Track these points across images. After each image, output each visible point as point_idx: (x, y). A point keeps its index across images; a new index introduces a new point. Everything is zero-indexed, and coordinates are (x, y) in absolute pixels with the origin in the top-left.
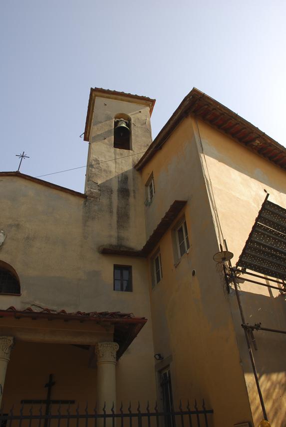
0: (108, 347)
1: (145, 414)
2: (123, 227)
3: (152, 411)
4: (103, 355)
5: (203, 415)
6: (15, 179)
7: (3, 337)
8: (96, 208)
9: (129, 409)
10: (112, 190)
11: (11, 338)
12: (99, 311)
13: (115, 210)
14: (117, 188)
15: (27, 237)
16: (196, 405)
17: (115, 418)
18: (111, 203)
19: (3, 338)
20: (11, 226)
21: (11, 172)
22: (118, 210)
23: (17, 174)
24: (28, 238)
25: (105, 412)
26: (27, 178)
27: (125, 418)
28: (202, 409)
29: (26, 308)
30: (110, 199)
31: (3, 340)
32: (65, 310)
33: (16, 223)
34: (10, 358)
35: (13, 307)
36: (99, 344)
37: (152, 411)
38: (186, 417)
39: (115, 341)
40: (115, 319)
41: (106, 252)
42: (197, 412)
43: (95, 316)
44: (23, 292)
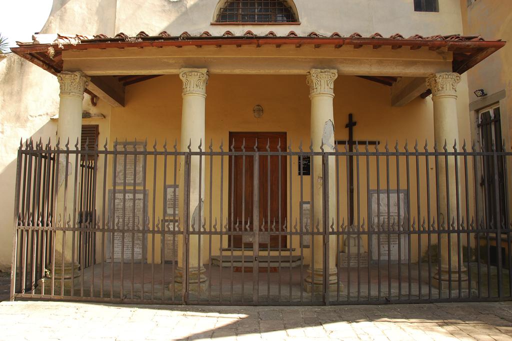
0: (448, 78)
1: (373, 153)
3: (469, 149)
7: (326, 70)
9: (425, 148)
11: (335, 71)
12: (443, 35)
17: (458, 157)
19: (325, 72)
25: (190, 150)
27: (410, 157)
29: (202, 32)
31: (327, 73)
32: (231, 31)
34: (206, 93)
35: (187, 33)
36: (438, 75)
38: (451, 159)
39: (454, 71)
40: (464, 43)
42: (407, 154)
43: (439, 39)
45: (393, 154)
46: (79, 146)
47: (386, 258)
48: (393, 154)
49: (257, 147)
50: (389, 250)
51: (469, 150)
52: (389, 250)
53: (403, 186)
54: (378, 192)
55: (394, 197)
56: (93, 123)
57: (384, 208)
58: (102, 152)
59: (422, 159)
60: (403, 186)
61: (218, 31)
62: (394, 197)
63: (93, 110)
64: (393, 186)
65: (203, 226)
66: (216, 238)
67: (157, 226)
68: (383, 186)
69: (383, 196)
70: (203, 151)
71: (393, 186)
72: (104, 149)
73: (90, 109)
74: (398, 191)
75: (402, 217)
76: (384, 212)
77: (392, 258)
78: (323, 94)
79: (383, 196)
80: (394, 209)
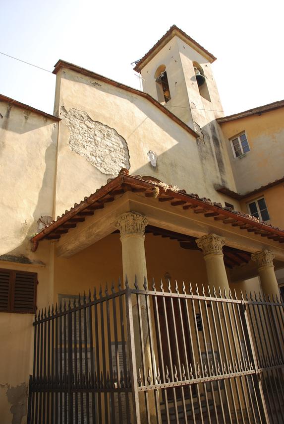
26: (156, 103)
56: (31, 270)
63: (31, 256)
73: (28, 254)
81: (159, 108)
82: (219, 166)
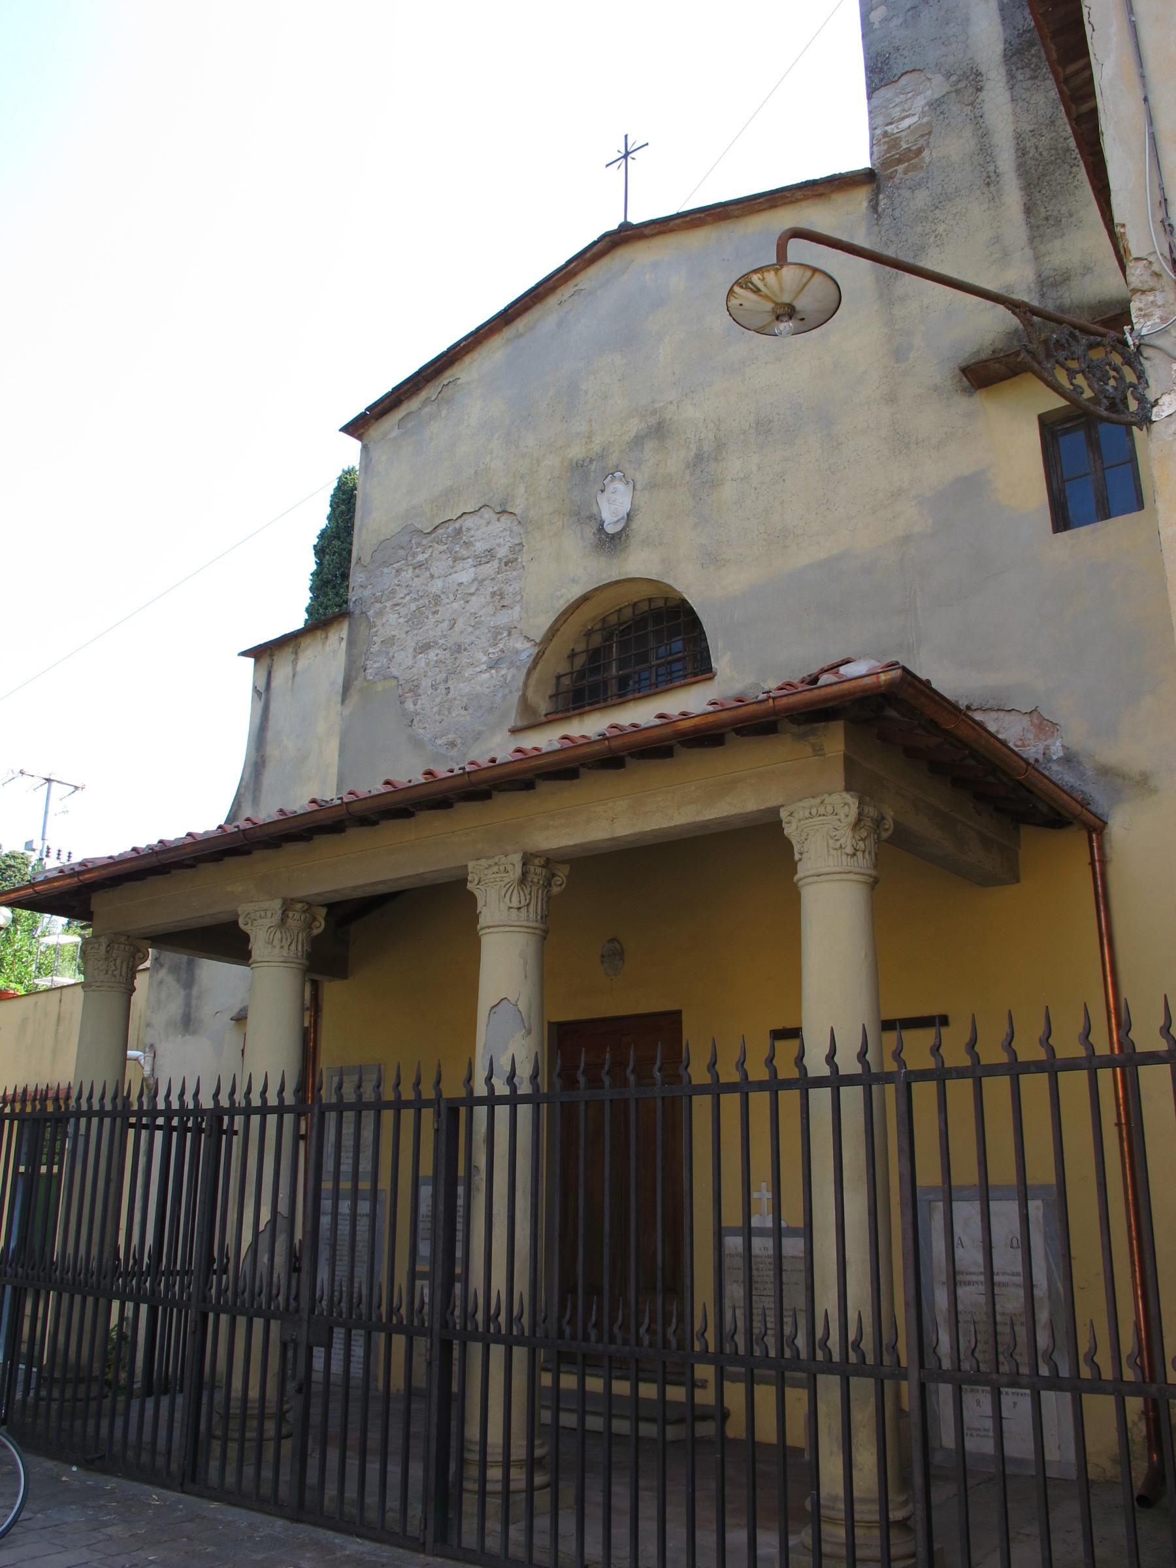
1: (1035, 1063)
2: (1058, 221)
3: (848, 1064)
4: (801, 854)
5: (1005, 1081)
6: (640, 255)
8: (921, 198)
10: (979, 74)
13: (1006, 161)
14: (999, 47)
15: (696, 456)
16: (973, 1042)
18: (983, 136)
20: (638, 441)
21: (595, 243)
22: (1021, 152)
23: (625, 236)
24: (699, 458)
26: (647, 231)
28: (791, 1073)
30: (978, 120)
33: (652, 421)
37: (848, 1064)
41: (983, 375)
42: (1015, 1069)
44: (721, 662)
45: (761, 1086)
46: (543, 1080)
47: (988, 1446)
48: (761, 1086)
49: (660, 1070)
50: (998, 1418)
51: (524, 1088)
52: (998, 1418)
53: (1041, 1172)
54: (949, 1195)
55: (1005, 1213)
57: (970, 1256)
58: (702, 1090)
59: (1034, 1086)
60: (1041, 1172)
61: (546, 740)
62: (1005, 1213)
64: (1002, 1171)
65: (1049, 1359)
66: (1099, 1407)
67: (1049, 1359)
68: (965, 1172)
69: (967, 1212)
70: (1102, 1049)
71: (1002, 1171)
72: (967, 1061)
74: (1023, 1193)
75: (1041, 1291)
76: (972, 1270)
77: (1011, 1449)
78: (489, 927)
79: (967, 1212)
80: (1007, 1260)
81: (672, 231)
82: (1028, 210)
